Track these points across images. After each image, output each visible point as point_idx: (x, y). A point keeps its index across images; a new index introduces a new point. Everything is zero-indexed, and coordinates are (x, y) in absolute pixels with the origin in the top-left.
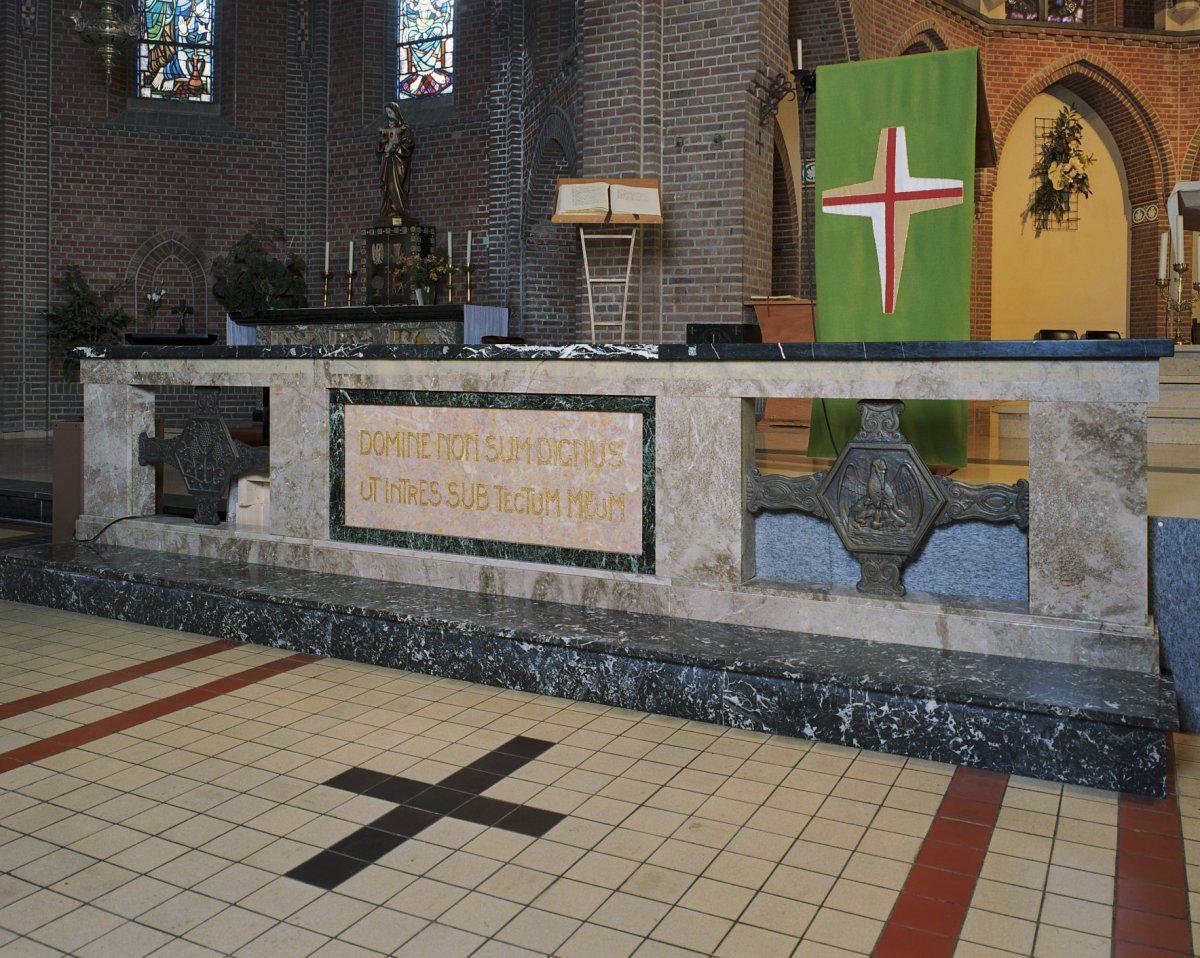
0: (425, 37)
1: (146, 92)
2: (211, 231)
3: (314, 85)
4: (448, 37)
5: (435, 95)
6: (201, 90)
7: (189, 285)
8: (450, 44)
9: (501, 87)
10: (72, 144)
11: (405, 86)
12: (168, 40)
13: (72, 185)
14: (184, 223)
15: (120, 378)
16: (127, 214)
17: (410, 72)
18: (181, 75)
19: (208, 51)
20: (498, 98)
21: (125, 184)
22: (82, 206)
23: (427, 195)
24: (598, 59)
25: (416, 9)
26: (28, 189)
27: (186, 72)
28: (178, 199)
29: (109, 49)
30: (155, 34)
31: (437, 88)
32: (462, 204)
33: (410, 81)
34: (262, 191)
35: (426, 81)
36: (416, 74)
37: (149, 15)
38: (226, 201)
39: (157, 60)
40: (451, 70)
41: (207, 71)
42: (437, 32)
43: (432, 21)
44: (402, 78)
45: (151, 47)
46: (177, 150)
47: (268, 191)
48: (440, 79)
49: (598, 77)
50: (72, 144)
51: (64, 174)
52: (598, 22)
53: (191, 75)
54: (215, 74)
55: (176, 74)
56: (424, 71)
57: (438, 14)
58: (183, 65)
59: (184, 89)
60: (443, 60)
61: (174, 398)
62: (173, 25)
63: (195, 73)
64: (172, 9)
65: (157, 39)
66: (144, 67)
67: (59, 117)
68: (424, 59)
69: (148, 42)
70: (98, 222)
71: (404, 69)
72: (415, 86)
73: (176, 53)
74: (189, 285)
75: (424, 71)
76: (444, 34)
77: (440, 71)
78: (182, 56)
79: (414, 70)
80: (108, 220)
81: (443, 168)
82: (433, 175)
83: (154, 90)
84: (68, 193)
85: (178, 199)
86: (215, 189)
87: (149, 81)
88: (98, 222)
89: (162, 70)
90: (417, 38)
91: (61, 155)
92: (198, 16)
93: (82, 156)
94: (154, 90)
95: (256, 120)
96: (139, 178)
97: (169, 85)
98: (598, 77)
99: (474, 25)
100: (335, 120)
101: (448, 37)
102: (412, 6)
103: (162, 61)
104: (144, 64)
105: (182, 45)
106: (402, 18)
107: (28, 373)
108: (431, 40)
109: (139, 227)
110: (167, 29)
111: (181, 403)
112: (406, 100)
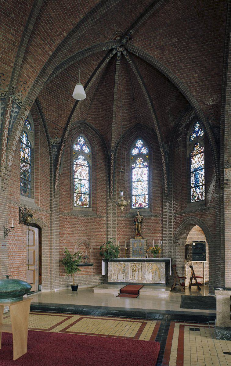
0: (140, 194)
1: (75, 205)
2: (92, 238)
3: (113, 204)
4: (146, 195)
5: (143, 208)
6: (87, 204)
7: (86, 251)
8: (147, 197)
9: (166, 208)
10: (63, 218)
11: (135, 205)
12: (80, 193)
13: (63, 228)
14: (86, 237)
15: (228, 294)
16: (75, 235)
17: (136, 202)
18: (82, 201)
19: (88, 195)
20: (165, 211)
21: (74, 228)
22: (65, 233)
23: (144, 231)
24: (228, 213)
25: (137, 188)
26: (55, 230)
27: (83, 200)
28: (85, 231)
29: (123, 207)
30: (77, 191)
31: (143, 206)
32: (154, 234)
33: (136, 204)
34: (102, 229)
35: (140, 204)
36: (137, 203)
37: (76, 187)
38: (95, 231)
39: (78, 197)
40: (147, 202)
41: (88, 200)
42: (143, 193)
43: (142, 191)
44: (134, 203)
45: (77, 194)
46: (85, 219)
47: (103, 229)
48: (144, 204)
49: (228, 217)
50: (63, 218)
51: (62, 225)
52: (227, 206)
53: (85, 201)
54: (90, 201)
55: (82, 201)
56: (139, 202)
57: (143, 189)
58: (83, 198)
59: (83, 204)
60: (145, 200)
61: (84, 279)
62: (81, 189)
63: (85, 200)
64: (80, 185)
65: (78, 192)
66: (75, 199)
67: (61, 212)
68: (140, 199)
69: (76, 193)
70: (69, 237)
71: (134, 201)
72: (137, 205)
73: (82, 196)
74: (86, 251)
75: (139, 202)
76: (145, 194)
77: (144, 202)
78: (83, 196)
79: (137, 202)
80: (71, 236)
81: (149, 225)
82: (146, 227)
83: (77, 205)
84: (62, 230)
85: (85, 231)
86: (93, 228)
87: (76, 202)
88: (69, 237)
89: (79, 200)
90: (138, 194)
91: (61, 221)
92: (86, 187)
93: (65, 221)
94: (77, 205)
95: (101, 212)
96: (77, 226)
97: (80, 203)
98: (228, 217)
99: (157, 194)
100: (118, 212)
101: (146, 195)
102: (136, 187)
103: (79, 197)
104: (75, 198)
105: (83, 194)
106: (133, 189)
107: (56, 275)
108: (142, 195)
109: (77, 238)
110: (80, 190)
111: (86, 280)
112: (135, 208)
